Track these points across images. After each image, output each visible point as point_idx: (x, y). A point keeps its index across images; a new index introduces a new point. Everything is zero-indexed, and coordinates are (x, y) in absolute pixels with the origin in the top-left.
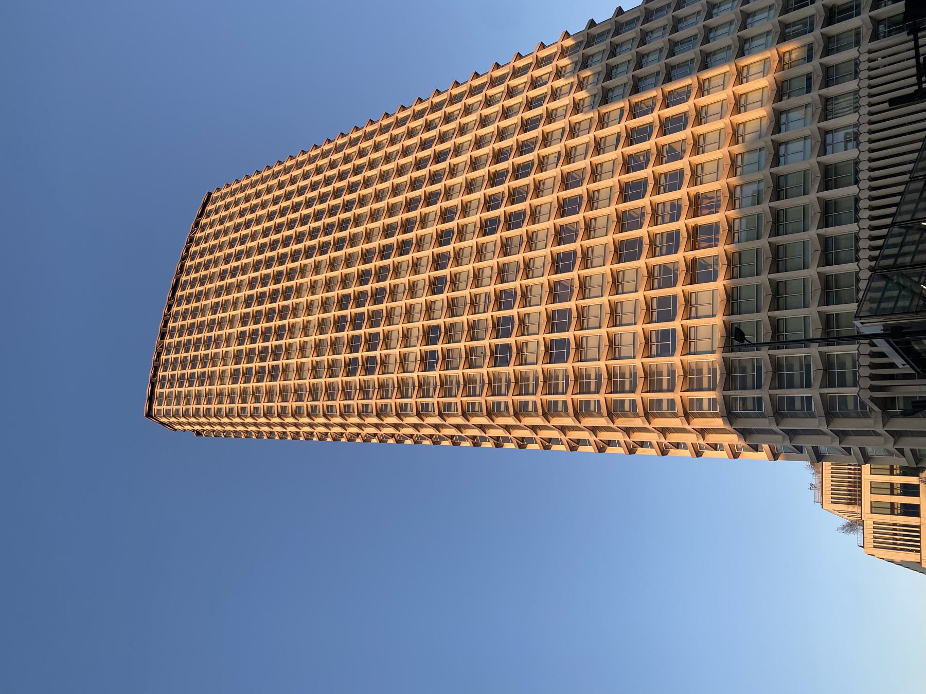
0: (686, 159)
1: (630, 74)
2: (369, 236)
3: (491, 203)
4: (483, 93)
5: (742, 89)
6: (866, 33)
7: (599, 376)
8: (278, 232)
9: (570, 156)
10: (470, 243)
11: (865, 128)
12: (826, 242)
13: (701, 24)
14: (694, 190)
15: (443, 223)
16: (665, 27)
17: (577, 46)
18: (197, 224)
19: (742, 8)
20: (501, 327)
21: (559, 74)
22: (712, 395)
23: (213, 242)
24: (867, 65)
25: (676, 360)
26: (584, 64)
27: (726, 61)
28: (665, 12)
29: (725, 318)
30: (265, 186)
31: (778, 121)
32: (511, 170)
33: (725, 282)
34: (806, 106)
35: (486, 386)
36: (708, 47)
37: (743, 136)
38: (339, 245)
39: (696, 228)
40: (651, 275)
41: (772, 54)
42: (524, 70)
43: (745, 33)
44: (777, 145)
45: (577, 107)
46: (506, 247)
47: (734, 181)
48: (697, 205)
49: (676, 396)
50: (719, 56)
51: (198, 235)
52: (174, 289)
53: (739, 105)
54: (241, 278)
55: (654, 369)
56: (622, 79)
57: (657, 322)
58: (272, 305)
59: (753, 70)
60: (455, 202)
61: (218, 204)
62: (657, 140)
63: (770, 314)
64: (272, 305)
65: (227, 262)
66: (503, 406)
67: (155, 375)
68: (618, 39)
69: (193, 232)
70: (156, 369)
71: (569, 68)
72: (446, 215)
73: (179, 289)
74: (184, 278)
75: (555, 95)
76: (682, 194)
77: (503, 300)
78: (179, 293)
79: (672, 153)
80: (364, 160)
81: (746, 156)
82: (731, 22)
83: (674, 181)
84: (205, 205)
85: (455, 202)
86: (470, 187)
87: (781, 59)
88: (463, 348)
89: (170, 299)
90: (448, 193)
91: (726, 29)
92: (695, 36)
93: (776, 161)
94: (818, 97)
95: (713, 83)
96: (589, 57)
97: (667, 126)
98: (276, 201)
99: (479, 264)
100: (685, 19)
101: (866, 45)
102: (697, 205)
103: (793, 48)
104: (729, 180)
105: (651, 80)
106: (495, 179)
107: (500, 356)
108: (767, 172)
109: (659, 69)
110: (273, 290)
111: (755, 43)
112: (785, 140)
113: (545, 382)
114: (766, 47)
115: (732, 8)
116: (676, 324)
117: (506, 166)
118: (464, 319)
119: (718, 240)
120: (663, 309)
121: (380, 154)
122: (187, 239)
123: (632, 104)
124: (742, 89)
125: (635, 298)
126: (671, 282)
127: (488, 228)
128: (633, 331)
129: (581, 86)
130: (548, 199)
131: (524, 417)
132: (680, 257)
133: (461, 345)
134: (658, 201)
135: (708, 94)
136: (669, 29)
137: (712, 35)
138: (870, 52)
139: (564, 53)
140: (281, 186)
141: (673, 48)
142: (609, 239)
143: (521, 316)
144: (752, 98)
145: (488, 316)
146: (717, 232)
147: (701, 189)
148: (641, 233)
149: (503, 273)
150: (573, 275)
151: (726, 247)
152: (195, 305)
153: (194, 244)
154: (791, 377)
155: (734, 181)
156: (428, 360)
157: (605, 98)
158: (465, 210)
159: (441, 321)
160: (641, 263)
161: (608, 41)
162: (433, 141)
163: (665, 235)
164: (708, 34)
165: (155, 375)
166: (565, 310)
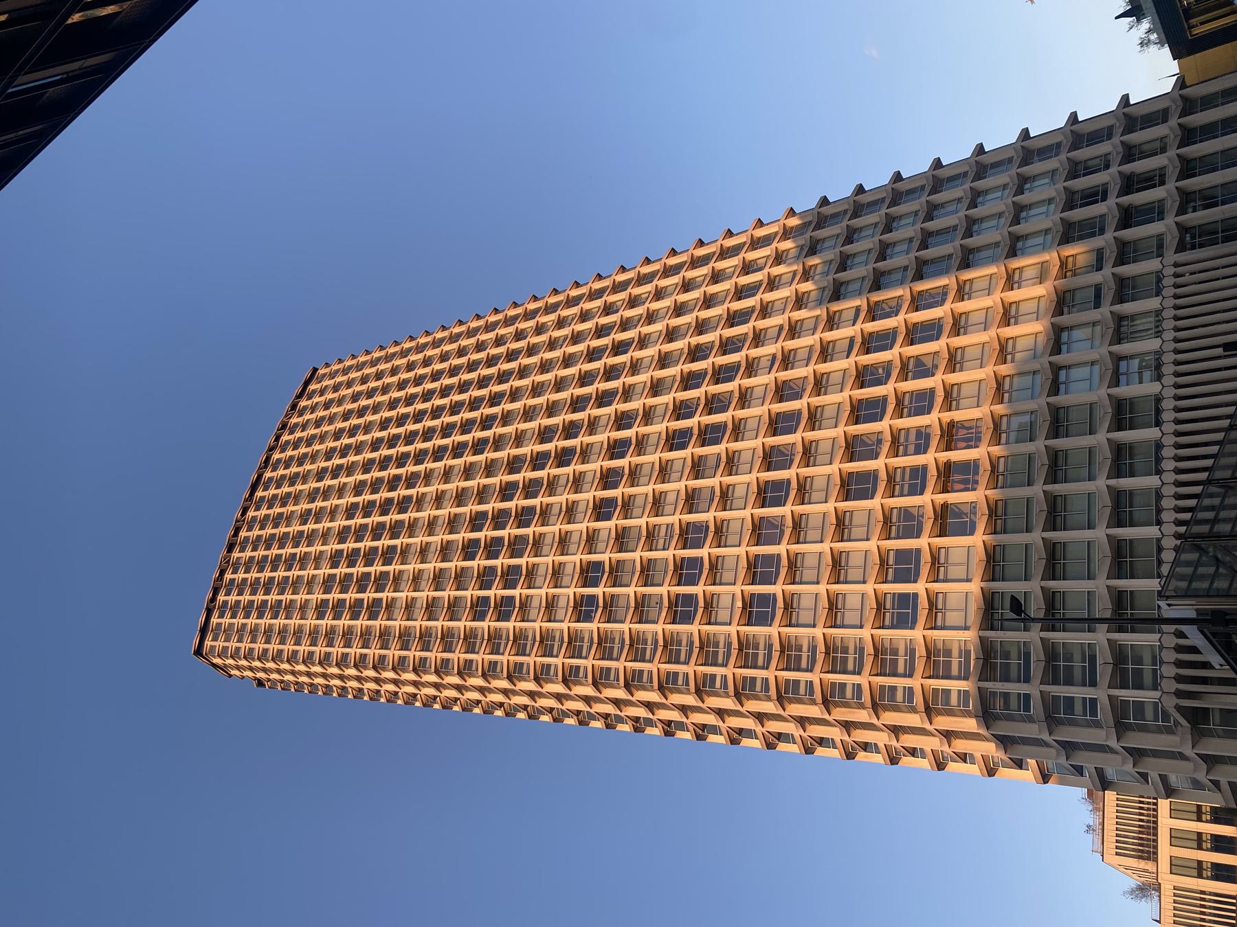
2: (519, 439)
5: (1013, 296)
6: (1171, 241)
10: (651, 458)
13: (962, 214)
14: (947, 416)
18: (294, 407)
20: (686, 571)
21: (779, 259)
22: (963, 685)
24: (1172, 323)
25: (917, 635)
26: (813, 250)
27: (993, 260)
29: (983, 584)
31: (1057, 339)
34: (1093, 363)
39: (948, 465)
40: (887, 520)
41: (1052, 257)
44: (1056, 369)
49: (916, 683)
50: (984, 254)
53: (1008, 316)
60: (635, 405)
61: (325, 383)
63: (1044, 583)
67: (213, 599)
70: (216, 591)
71: (792, 253)
72: (623, 421)
73: (261, 488)
76: (932, 420)
77: (690, 536)
78: (259, 493)
79: (921, 368)
81: (1016, 380)
82: (1000, 215)
83: (922, 403)
86: (656, 388)
87: (1063, 264)
90: (627, 393)
91: (1044, 209)
92: (955, 228)
93: (1055, 389)
95: (976, 286)
99: (661, 487)
100: (942, 205)
101: (1171, 257)
102: (951, 435)
107: (681, 609)
111: (1030, 242)
112: (1066, 363)
116: (919, 588)
118: (637, 556)
119: (976, 482)
122: (278, 425)
124: (1013, 296)
125: (865, 548)
127: (676, 440)
128: (860, 592)
129: (806, 275)
130: (757, 412)
132: (927, 500)
133: (630, 591)
134: (901, 427)
139: (787, 234)
141: (926, 240)
142: (834, 469)
146: (976, 472)
148: (883, 426)
149: (692, 501)
157: (837, 293)
158: (648, 416)
160: (875, 503)
163: (908, 470)
164: (970, 228)
165: (213, 599)
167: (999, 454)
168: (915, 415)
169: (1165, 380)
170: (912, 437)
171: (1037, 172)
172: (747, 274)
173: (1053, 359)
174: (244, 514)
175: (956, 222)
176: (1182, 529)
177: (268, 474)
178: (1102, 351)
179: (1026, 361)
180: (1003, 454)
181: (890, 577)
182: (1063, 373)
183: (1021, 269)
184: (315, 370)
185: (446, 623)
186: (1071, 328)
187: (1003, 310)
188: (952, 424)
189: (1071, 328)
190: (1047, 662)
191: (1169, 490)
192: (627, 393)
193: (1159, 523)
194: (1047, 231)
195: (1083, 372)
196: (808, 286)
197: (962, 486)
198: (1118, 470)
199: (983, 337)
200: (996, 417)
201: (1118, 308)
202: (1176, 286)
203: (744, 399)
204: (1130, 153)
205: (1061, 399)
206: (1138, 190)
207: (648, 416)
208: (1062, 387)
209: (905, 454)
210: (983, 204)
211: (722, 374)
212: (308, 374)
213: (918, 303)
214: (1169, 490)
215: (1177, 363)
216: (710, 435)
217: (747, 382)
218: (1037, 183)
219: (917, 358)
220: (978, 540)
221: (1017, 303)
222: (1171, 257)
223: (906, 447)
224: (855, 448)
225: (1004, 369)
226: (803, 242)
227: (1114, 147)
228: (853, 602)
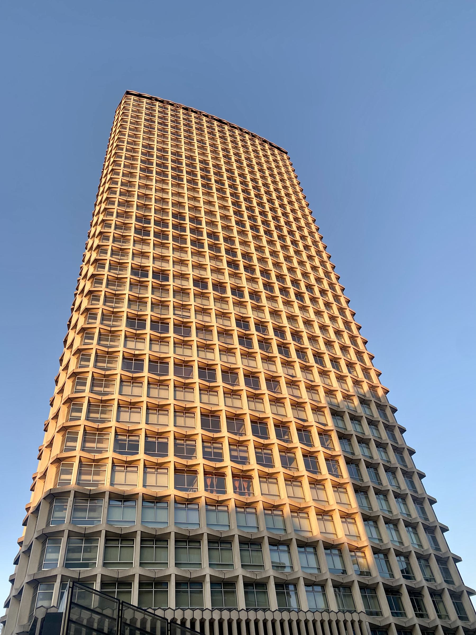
0: (282, 470)
1: (353, 432)
2: (244, 243)
3: (261, 326)
4: (364, 379)
5: (337, 516)
6: (377, 621)
7: (103, 421)
8: (260, 213)
9: (292, 384)
10: (231, 309)
11: (294, 617)
12: (197, 583)
13: (390, 488)
14: (255, 475)
15: (249, 293)
16: (409, 515)
17: (379, 399)
18: (265, 141)
19: (401, 520)
20: (160, 325)
21: (357, 383)
22: (73, 481)
23: (251, 148)
24: (349, 619)
25: (110, 454)
26: (364, 401)
27: (360, 506)
28: (422, 515)
29: (141, 495)
30: (288, 185)
31: (306, 545)
32: (312, 450)
33: (172, 497)
34: (319, 569)
35: (100, 397)
36: (372, 493)
37: (297, 517)
38: (240, 223)
39: (223, 475)
40: (188, 437)
41: (364, 541)
42: (354, 342)
43: (381, 522)
44: (287, 543)
45: (330, 392)
46: (225, 333)
47: (260, 507)
48: (243, 477)
49: (78, 453)
50: (364, 501)
51: (257, 142)
52: (219, 121)
53: (323, 514)
54: (230, 200)
55: (106, 437)
56: (350, 427)
57: (146, 442)
58: (206, 246)
59: (352, 527)
60: (264, 301)
61: (278, 156)
62: (306, 477)
63: (139, 534)
64: (206, 246)
65: (247, 208)
66: (93, 321)
67: (157, 100)
68: (381, 427)
69: (259, 139)
70: (162, 102)
71: (361, 391)
72: (255, 295)
73: (219, 124)
74: (226, 127)
75: (341, 378)
76: (253, 465)
77: (182, 327)
78: (216, 123)
79: (288, 461)
80: (318, 294)
81: (281, 518)
82: (390, 512)
83: (264, 459)
84: (278, 149)
85: (264, 301)
86: (275, 313)
87: (359, 549)
88: (139, 427)
89: (212, 117)
90: (272, 299)
91: (396, 539)
92: (381, 484)
93: (274, 543)
94: (325, 578)
95: (343, 496)
96: (369, 405)
97: (310, 458)
98: (288, 223)
99: (215, 314)
100: (395, 477)
101: (367, 620)
102: (243, 477)
103: (368, 559)
104: (261, 503)
105: (348, 449)
106: (279, 331)
107: (136, 321)
108: (265, 533)
109: (356, 454)
110: (218, 236)
111: (373, 530)
112: (292, 551)
113: (98, 429)
114: (370, 538)
115: (402, 513)
116: (141, 455)
117: (288, 339)
118: (171, 298)
119: (212, 492)
120: (156, 444)
121: (322, 308)
122: (254, 133)
123: (337, 458)
124: (337, 516)
125: (168, 424)
126: (178, 452)
127: (242, 322)
128: (139, 421)
129: (347, 397)
130: (259, 366)
131: (63, 436)
132: (199, 461)
133: (149, 295)
134: (249, 447)
135: (334, 491)
136: (408, 519)
137: (391, 526)
138: (360, 622)
139: (373, 388)
140: (290, 203)
141: (371, 466)
142: (222, 406)
143: (167, 340)
144: (329, 526)
145: (171, 315)
146: (218, 492)
147: (256, 481)
148: (224, 432)
149: (204, 329)
150: (196, 379)
151: (203, 499)
152: (208, 143)
153: (251, 137)
154: (78, 550)
155: (260, 507)
156: (140, 271)
157: (336, 414)
158: (258, 309)
159: (171, 283)
160: (199, 430)
161: (380, 419)
162: (338, 369)
163: (220, 451)
164: (381, 493)
165: (157, 100)
166: (167, 450)
167: (284, 511)
168: (256, 456)
169: (340, 614)
170: (243, 454)
171: (420, 535)
172: (347, 366)
173: (294, 542)
174: (246, 132)
175: (365, 480)
176: (188, 625)
177: (226, 127)
178: (327, 575)
179: (293, 524)
180: (285, 515)
181: (150, 439)
182: (285, 548)
183: (355, 523)
184: (286, 153)
185: (135, 203)
186: (316, 554)
187: (330, 512)
188: (250, 478)
189: (316, 554)
190: (120, 535)
191: (269, 616)
192: (272, 299)
193: (247, 610)
194: (381, 540)
195: (313, 563)
196: (339, 397)
197: (209, 483)
198: (216, 583)
199: (284, 494)
200: (281, 507)
201: (330, 583)
202: (345, 622)
203: (268, 360)
204: (436, 595)
205: (266, 546)
206: (412, 600)
207: (258, 309)
208: (302, 549)
209: (230, 450)
210: (397, 502)
211: (283, 348)
212: (283, 149)
213: (331, 460)
214: (269, 616)
215: (290, 622)
216: (245, 340)
217: (278, 361)
218: (413, 535)
219: (294, 459)
220: (172, 491)
221: (332, 520)
222: (367, 620)
223: (236, 450)
224: (235, 420)
225: (287, 510)
226: (367, 396)
227: (440, 584)
228: (135, 417)
